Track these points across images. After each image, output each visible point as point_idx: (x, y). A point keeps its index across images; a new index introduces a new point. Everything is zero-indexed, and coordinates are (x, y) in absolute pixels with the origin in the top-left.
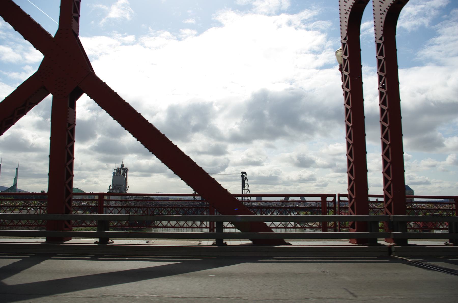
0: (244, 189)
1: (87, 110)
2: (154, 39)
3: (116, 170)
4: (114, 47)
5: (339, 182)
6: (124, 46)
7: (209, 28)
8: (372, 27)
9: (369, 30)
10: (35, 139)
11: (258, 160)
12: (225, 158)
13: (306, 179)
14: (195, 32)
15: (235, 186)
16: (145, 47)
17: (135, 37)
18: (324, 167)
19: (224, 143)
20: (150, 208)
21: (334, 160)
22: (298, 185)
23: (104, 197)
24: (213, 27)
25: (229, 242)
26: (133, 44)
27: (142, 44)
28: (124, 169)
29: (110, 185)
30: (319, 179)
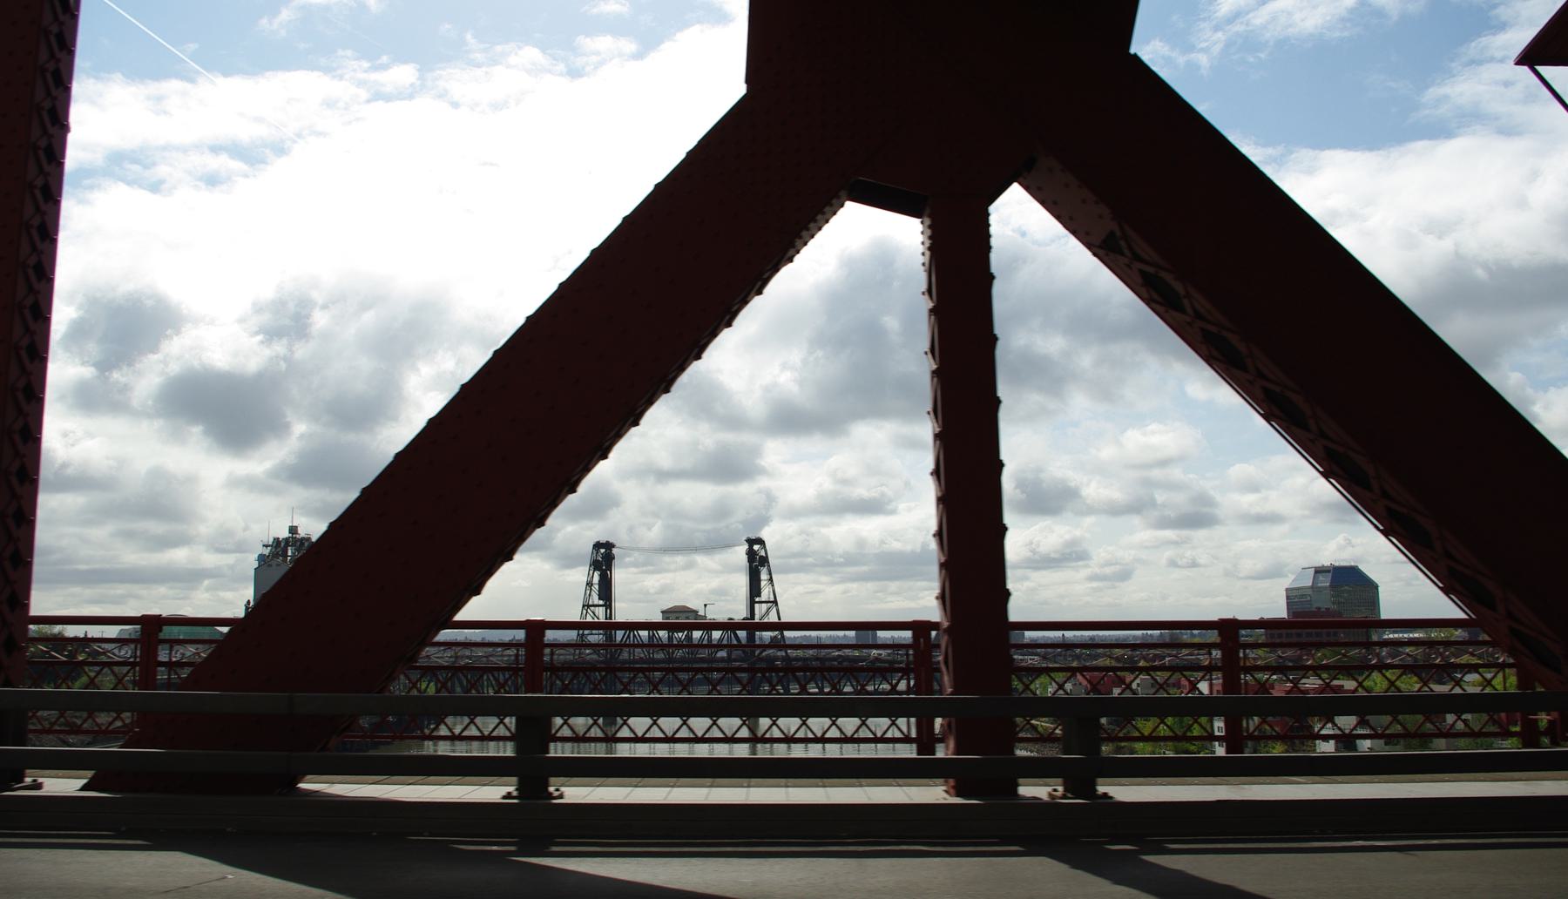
0: (757, 599)
1: (251, 336)
2: (487, 73)
3: (269, 546)
4: (346, 109)
5: (1173, 564)
6: (381, 102)
7: (680, 29)
8: (1260, 5)
9: (1251, 15)
10: (73, 445)
11: (874, 494)
12: (760, 491)
13: (1053, 555)
14: (630, 46)
15: (800, 589)
16: (456, 105)
17: (419, 70)
18: (1115, 510)
19: (746, 438)
20: (647, 673)
21: (1148, 483)
22: (1026, 578)
23: (544, 635)
24: (693, 25)
25: (784, 789)
26: (408, 94)
27: (442, 95)
28: (299, 543)
29: (249, 602)
30: (1100, 554)
